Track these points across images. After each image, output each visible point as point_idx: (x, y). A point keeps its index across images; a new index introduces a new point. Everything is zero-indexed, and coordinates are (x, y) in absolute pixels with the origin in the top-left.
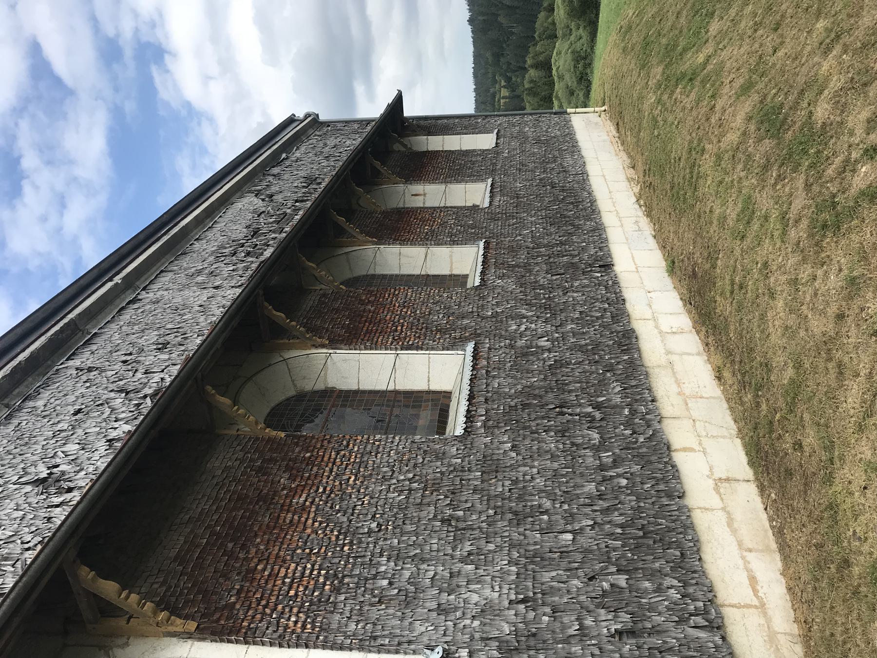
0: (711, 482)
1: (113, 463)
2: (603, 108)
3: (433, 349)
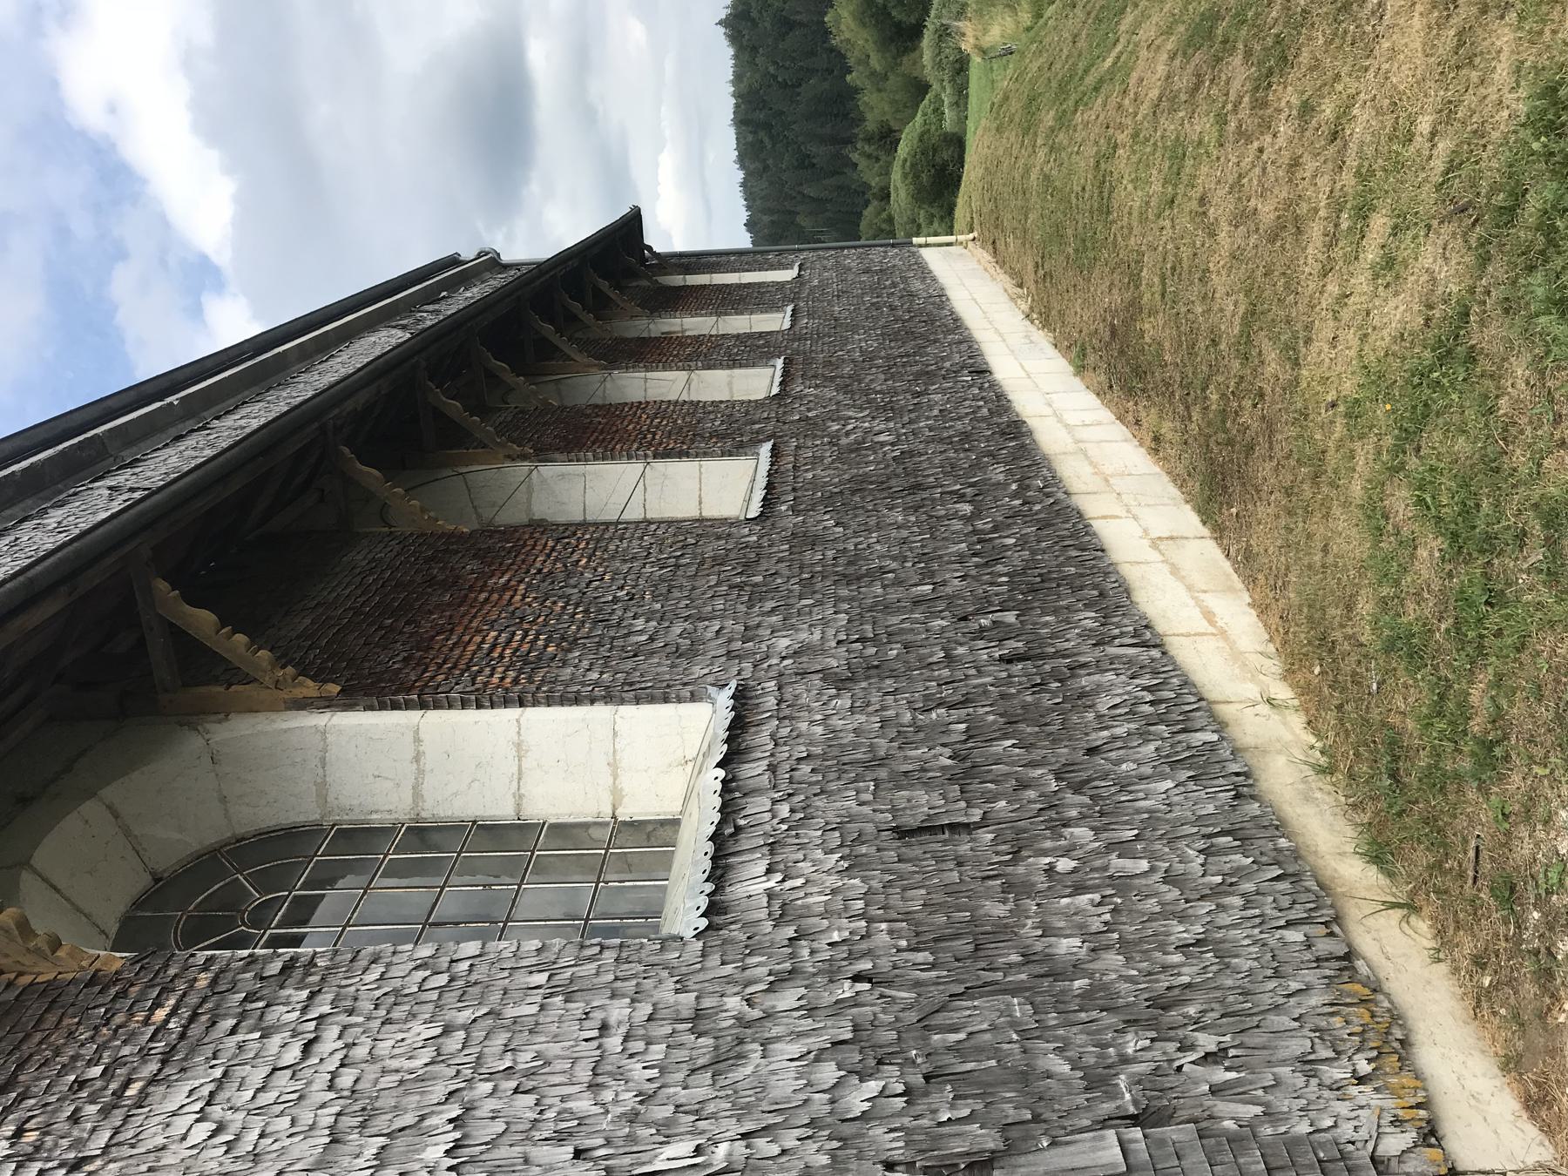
0: (1146, 543)
1: (203, 469)
2: (971, 236)
3: (705, 454)
